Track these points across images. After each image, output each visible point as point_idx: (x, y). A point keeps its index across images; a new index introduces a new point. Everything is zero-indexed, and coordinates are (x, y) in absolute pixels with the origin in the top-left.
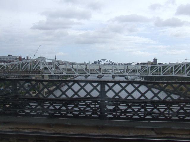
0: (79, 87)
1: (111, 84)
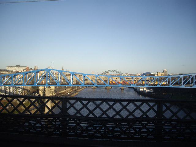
0: (148, 108)
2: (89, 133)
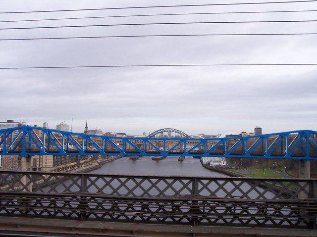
0: (217, 187)
1: (205, 182)
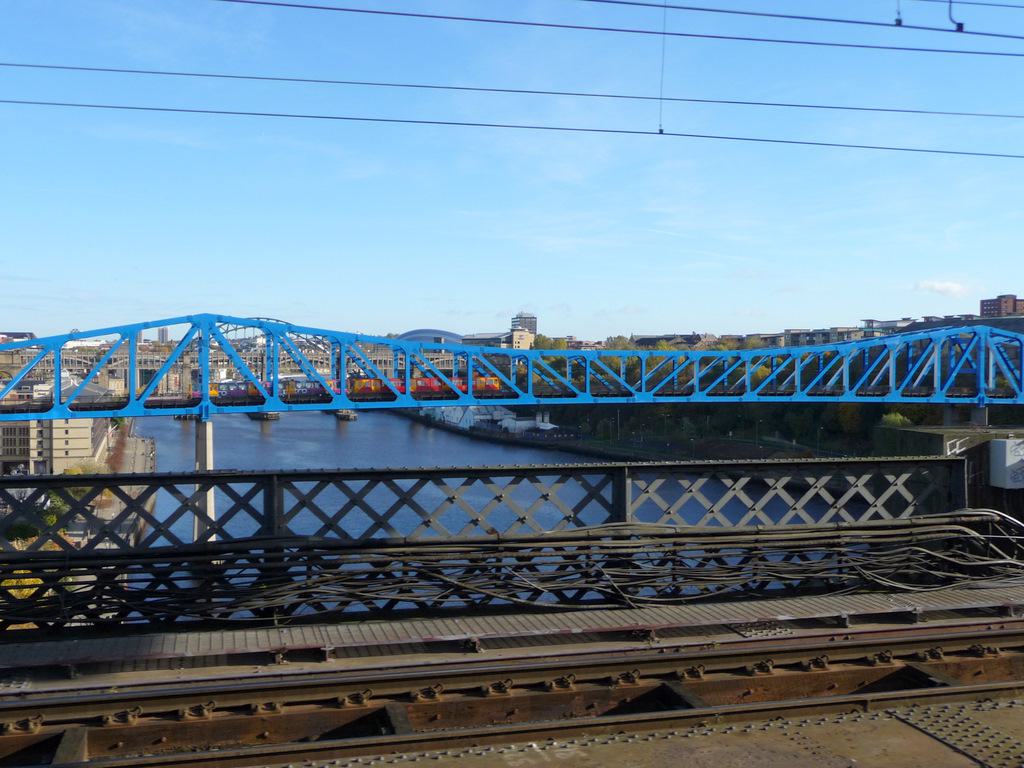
0: (394, 498)
1: (305, 487)
2: (157, 565)
